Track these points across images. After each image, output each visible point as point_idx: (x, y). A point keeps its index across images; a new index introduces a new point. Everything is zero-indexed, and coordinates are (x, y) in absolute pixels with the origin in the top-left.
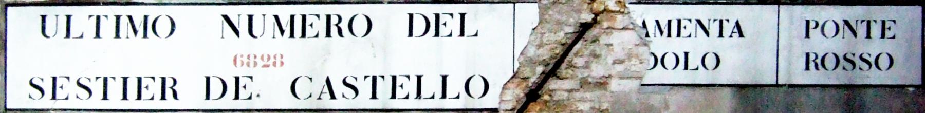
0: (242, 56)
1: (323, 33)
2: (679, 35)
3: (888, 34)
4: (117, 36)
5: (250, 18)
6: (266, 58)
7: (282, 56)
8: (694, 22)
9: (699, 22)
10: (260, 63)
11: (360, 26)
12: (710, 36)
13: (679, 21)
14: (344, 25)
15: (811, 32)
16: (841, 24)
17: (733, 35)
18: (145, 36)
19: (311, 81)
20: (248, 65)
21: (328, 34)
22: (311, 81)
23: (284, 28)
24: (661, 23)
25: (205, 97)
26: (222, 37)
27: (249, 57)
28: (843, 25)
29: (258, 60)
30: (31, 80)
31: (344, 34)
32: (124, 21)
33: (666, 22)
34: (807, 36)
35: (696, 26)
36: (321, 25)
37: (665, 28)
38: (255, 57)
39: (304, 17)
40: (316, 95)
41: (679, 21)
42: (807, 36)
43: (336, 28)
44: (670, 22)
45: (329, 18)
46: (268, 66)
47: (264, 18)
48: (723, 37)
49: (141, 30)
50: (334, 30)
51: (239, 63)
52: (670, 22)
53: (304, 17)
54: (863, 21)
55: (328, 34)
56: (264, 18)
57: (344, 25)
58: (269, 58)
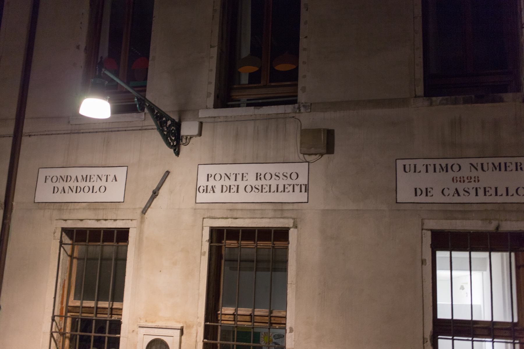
0: (456, 178)
2: (506, 170)
3: (508, 169)
6: (469, 178)
7: (478, 177)
8: (96, 176)
9: (98, 176)
10: (466, 181)
13: (90, 176)
14: (262, 176)
15: (210, 178)
16: (59, 177)
20: (460, 181)
21: (517, 170)
24: (473, 164)
25: (509, 188)
26: (225, 181)
27: (460, 178)
29: (465, 179)
33: (498, 164)
34: (208, 180)
35: (97, 179)
36: (513, 167)
37: (445, 168)
38: (463, 177)
39: (505, 164)
41: (90, 176)
42: (208, 180)
44: (87, 176)
45: (516, 164)
46: (471, 182)
51: (455, 181)
52: (87, 176)
53: (505, 164)
57: (262, 176)
58: (471, 178)
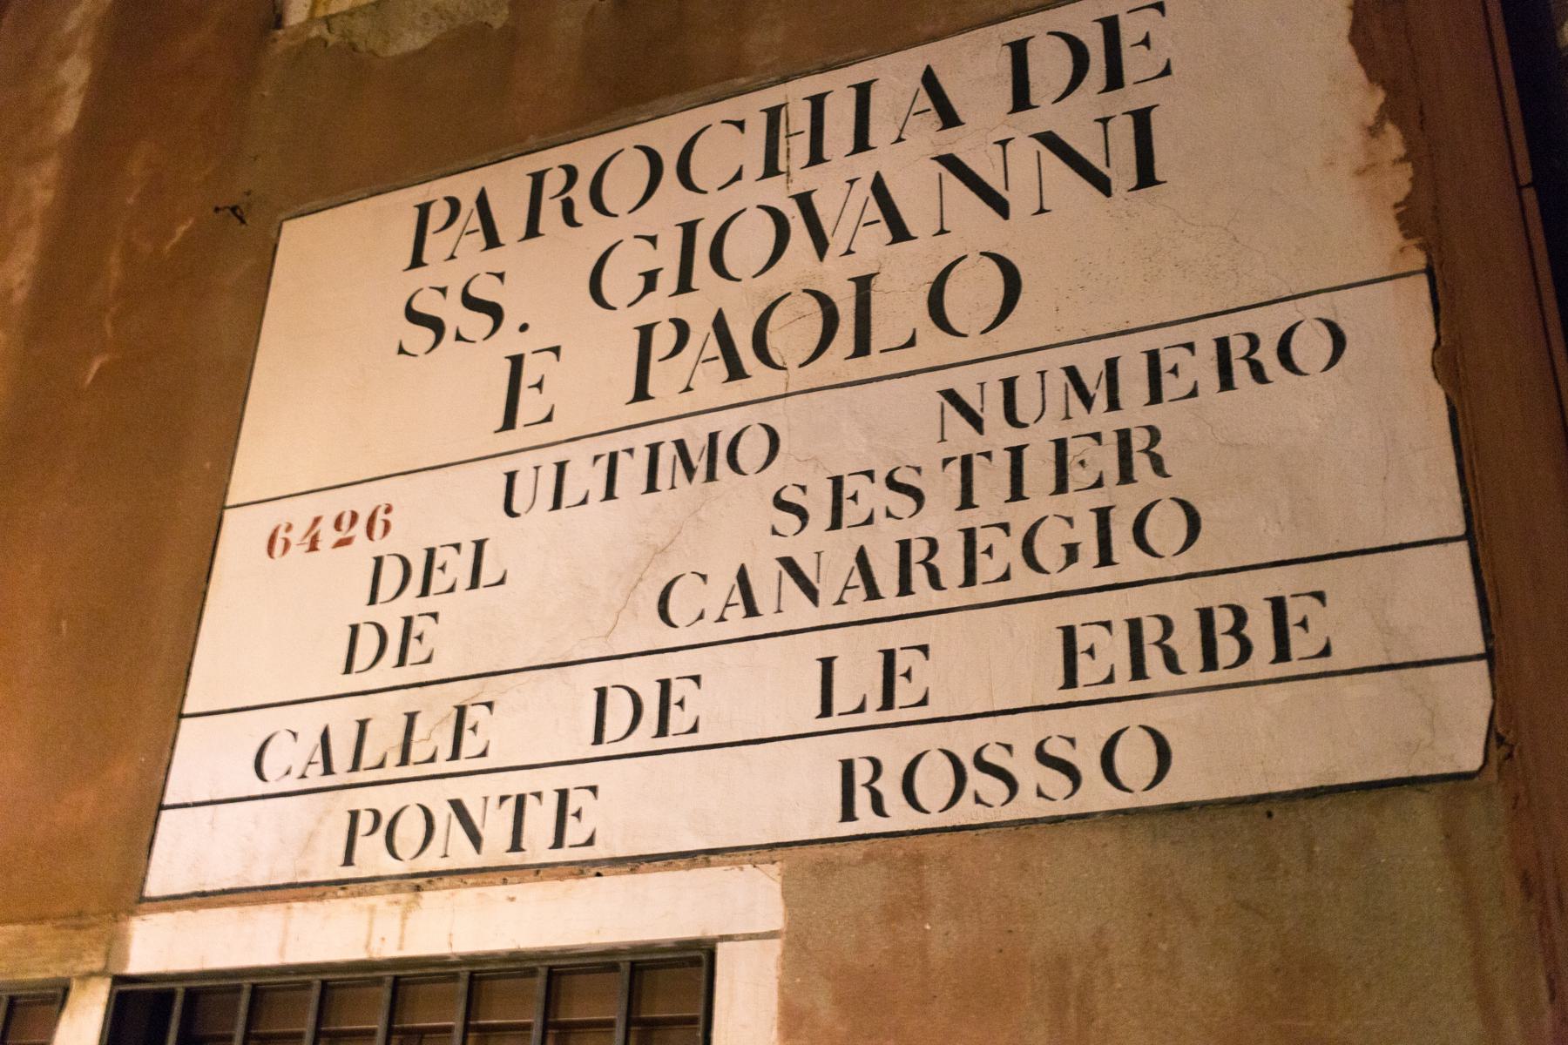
1: (1211, 378)
4: (652, 487)
5: (1009, 385)
11: (1311, 347)
12: (856, 550)
14: (1267, 356)
17: (729, 613)
18: (711, 476)
19: (1072, 526)
21: (1227, 383)
22: (1072, 526)
23: (1091, 391)
28: (445, 818)
30: (919, 507)
31: (1269, 373)
32: (667, 454)
40: (296, 772)
43: (1245, 365)
47: (537, 473)
48: (1066, 546)
49: (701, 466)
50: (1240, 370)
54: (503, 799)
55: (1227, 383)
56: (537, 473)
57: (1267, 356)
